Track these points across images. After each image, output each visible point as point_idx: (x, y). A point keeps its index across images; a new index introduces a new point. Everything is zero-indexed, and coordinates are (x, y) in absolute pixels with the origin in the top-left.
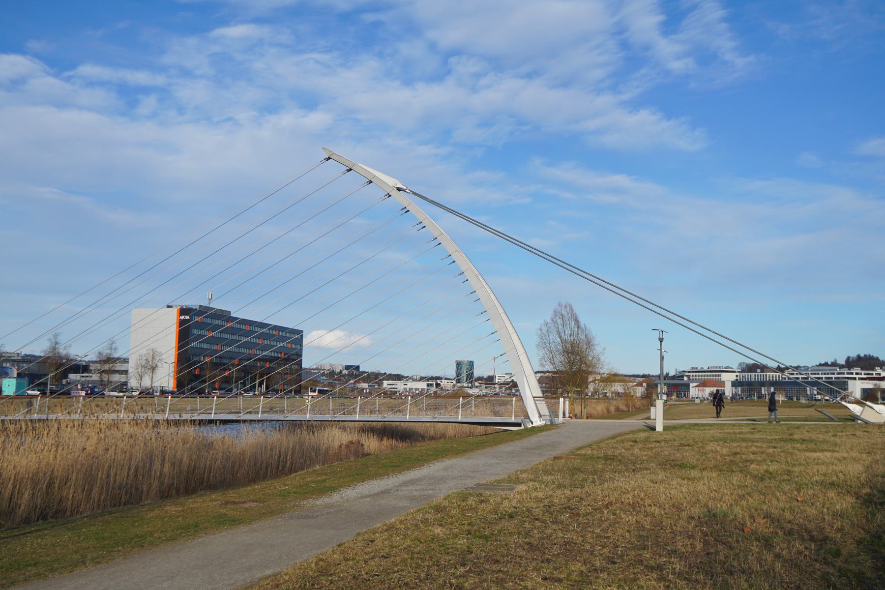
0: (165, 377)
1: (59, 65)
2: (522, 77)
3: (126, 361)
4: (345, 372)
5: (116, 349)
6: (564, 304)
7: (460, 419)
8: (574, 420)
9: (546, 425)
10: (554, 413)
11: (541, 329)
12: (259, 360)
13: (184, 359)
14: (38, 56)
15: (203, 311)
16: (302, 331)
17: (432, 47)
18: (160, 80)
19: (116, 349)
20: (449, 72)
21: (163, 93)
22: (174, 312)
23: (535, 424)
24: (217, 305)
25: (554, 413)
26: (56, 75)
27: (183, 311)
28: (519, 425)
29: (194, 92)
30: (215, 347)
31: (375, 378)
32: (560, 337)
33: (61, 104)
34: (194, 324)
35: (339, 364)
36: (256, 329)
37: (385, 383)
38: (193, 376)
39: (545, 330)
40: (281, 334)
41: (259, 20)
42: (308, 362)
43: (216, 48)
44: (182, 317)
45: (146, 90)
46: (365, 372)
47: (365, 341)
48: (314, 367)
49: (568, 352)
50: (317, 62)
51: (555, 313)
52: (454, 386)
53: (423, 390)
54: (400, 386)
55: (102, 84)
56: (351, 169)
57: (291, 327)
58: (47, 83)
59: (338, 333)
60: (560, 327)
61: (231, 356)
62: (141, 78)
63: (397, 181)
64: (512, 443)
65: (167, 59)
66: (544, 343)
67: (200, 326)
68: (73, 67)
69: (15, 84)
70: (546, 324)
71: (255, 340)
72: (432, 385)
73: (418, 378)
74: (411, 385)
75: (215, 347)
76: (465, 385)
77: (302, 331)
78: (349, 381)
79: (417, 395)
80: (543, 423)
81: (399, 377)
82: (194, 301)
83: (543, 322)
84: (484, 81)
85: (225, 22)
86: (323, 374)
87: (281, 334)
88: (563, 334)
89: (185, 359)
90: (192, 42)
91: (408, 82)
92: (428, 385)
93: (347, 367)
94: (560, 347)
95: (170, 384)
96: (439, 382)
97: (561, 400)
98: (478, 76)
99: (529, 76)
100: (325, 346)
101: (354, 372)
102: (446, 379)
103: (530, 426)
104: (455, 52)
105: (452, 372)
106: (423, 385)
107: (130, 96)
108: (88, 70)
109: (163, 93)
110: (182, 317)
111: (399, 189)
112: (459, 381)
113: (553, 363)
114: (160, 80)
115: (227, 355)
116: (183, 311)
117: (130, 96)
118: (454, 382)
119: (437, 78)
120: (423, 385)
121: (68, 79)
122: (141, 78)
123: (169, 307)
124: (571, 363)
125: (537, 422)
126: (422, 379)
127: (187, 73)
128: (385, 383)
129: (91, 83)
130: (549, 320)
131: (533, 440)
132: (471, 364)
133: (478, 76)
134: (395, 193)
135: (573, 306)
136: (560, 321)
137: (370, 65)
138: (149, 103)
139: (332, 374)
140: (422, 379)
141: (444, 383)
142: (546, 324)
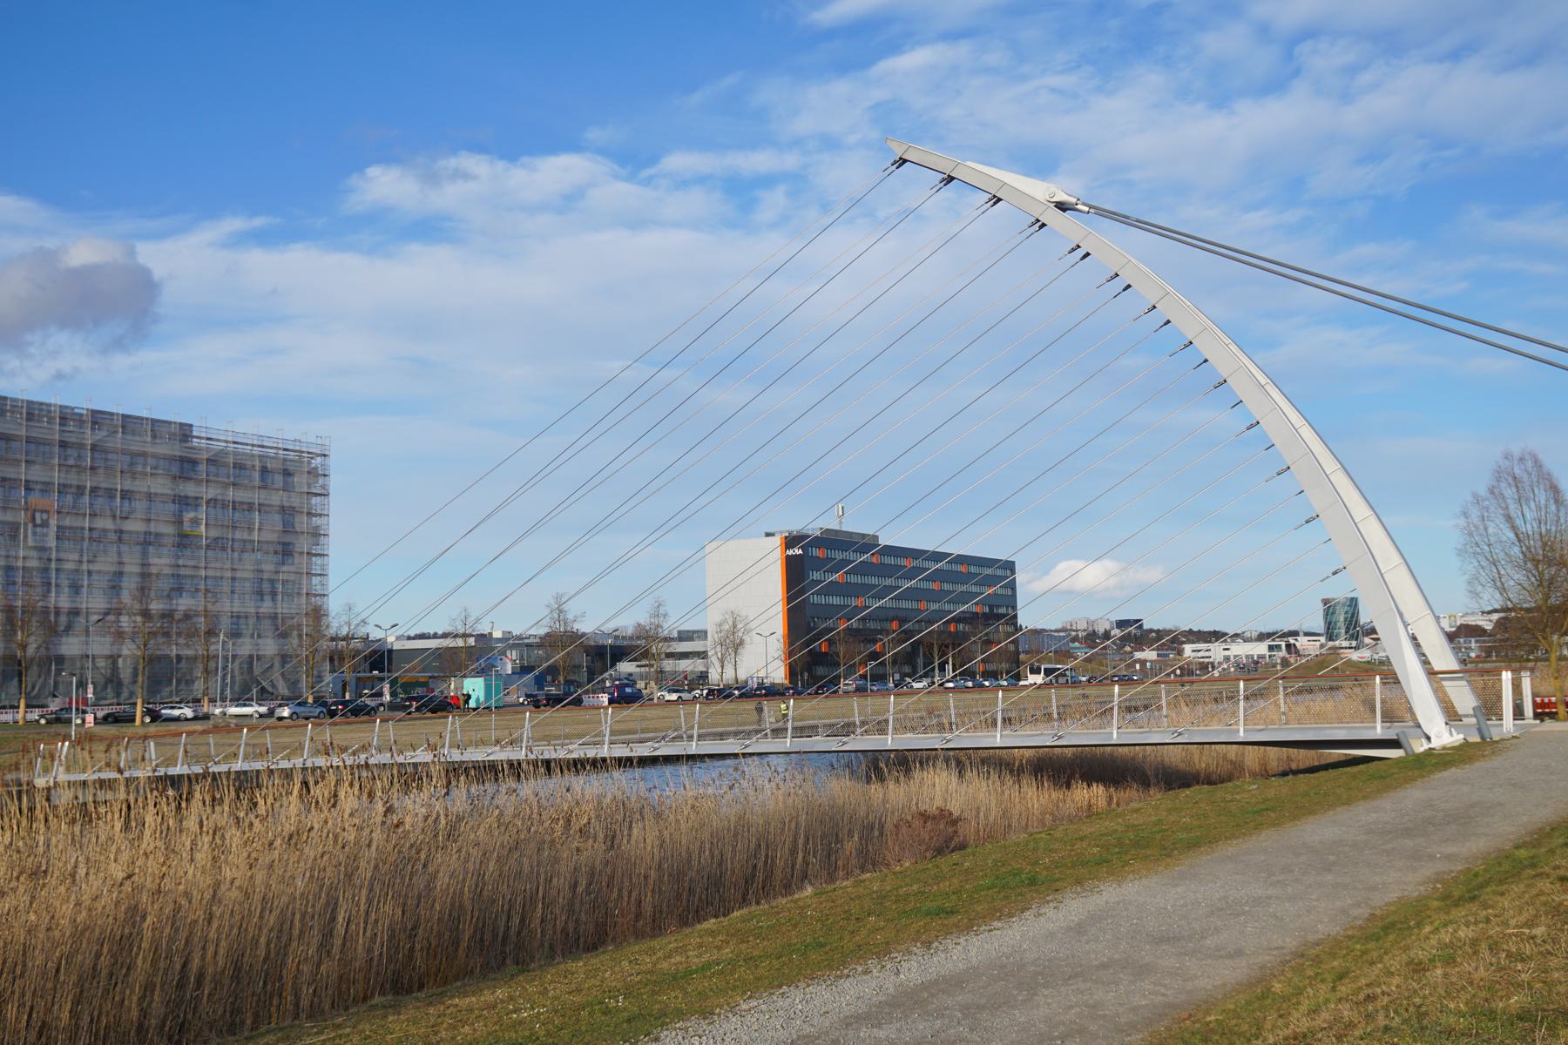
0: (764, 658)
1: (633, 161)
2: (1441, 60)
3: (703, 634)
4: (1116, 632)
5: (665, 615)
6: (1517, 452)
7: (1242, 735)
8: (1549, 725)
9: (1466, 744)
10: (1489, 707)
11: (1465, 514)
12: (957, 620)
13: (800, 621)
14: (603, 151)
15: (833, 541)
16: (1010, 566)
17: (1264, 31)
18: (791, 161)
19: (665, 615)
20: (1297, 72)
21: (797, 182)
22: (777, 541)
23: (1436, 743)
24: (851, 526)
25: (1489, 707)
26: (630, 178)
27: (790, 541)
28: (1394, 744)
29: (849, 173)
30: (854, 602)
31: (1171, 641)
32: (1514, 528)
33: (636, 222)
34: (810, 562)
35: (1104, 617)
36: (926, 564)
37: (1188, 649)
38: (822, 653)
39: (1475, 519)
40: (989, 571)
41: (953, 36)
42: (1029, 617)
43: (879, 94)
44: (790, 552)
45: (768, 181)
46: (1151, 631)
47: (1152, 574)
48: (1059, 626)
49: (1536, 562)
50: (1053, 90)
51: (1499, 474)
52: (1322, 646)
53: (1262, 657)
54: (1216, 652)
55: (701, 180)
56: (951, 179)
57: (931, 548)
58: (619, 192)
59: (1109, 565)
60: (1513, 507)
61: (883, 616)
62: (760, 161)
63: (1053, 188)
64: (1342, 814)
65: (804, 125)
66: (1475, 544)
67: (819, 564)
68: (653, 160)
69: (569, 201)
70: (1477, 499)
71: (925, 585)
72: (1279, 647)
73: (1254, 635)
74: (1240, 650)
75: (854, 602)
76: (1345, 644)
77: (1010, 566)
78: (1123, 652)
79: (1251, 669)
80: (1456, 738)
81: (1216, 636)
82: (813, 522)
83: (1469, 498)
84: (1366, 78)
85: (894, 48)
86: (1075, 639)
87: (989, 571)
88: (1519, 522)
89: (801, 622)
90: (841, 88)
91: (1220, 100)
92: (1271, 648)
93: (1121, 624)
94: (1516, 551)
95: (778, 674)
96: (1292, 640)
97: (1507, 676)
98: (1353, 70)
99: (1455, 56)
100: (1064, 588)
101: (1135, 634)
102: (1307, 634)
103: (1420, 747)
104: (1309, 33)
105: (1318, 624)
106: (1261, 649)
107: (742, 192)
108: (679, 161)
109: (797, 182)
110: (790, 552)
111: (1062, 207)
112: (1330, 639)
113: (1503, 590)
114: (791, 161)
115: (877, 617)
116: (790, 541)
117: (742, 192)
118: (1323, 639)
119: (1273, 86)
120: (1261, 649)
121: (648, 182)
122: (760, 161)
123: (768, 535)
124: (1546, 585)
125: (1442, 736)
126: (1262, 637)
127: (830, 143)
128: (1188, 649)
129: (683, 183)
130: (1483, 492)
131: (1414, 796)
132: (1353, 603)
133: (1353, 70)
134: (1053, 217)
135: (1541, 457)
136: (1510, 492)
137: (1149, 80)
138: (774, 201)
139: (1091, 638)
140: (1262, 637)
141: (1302, 642)
142: (1477, 499)
